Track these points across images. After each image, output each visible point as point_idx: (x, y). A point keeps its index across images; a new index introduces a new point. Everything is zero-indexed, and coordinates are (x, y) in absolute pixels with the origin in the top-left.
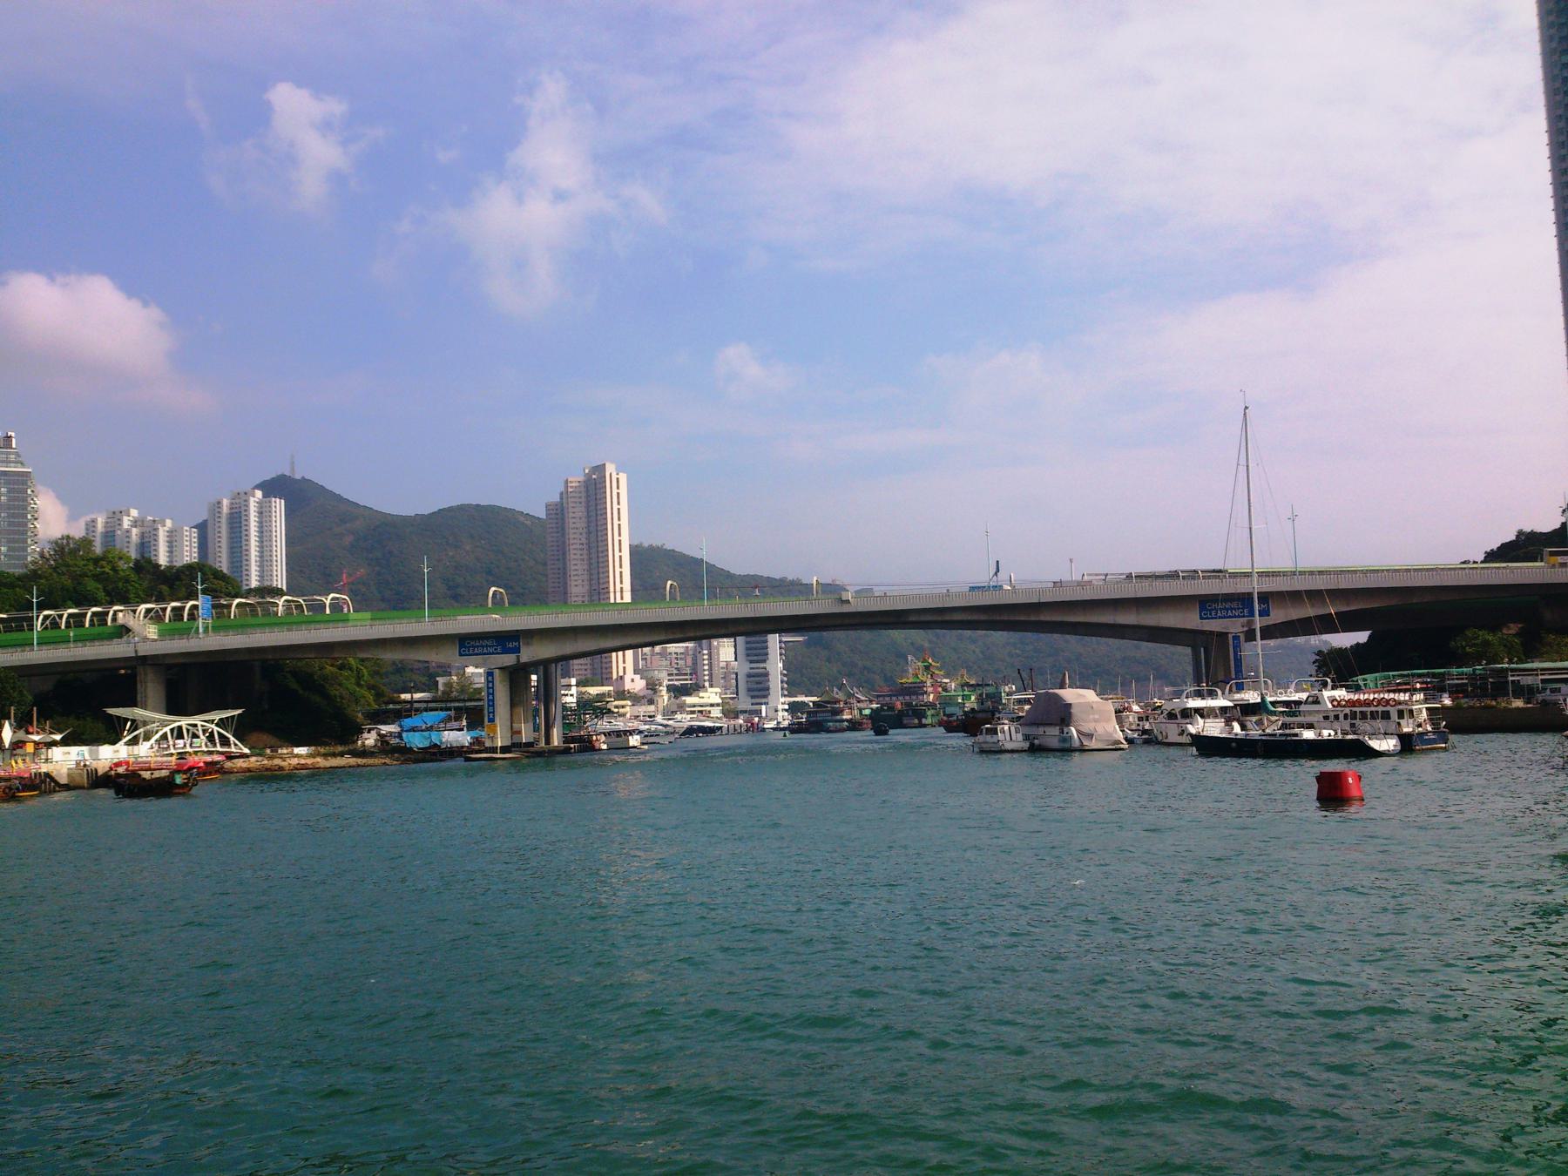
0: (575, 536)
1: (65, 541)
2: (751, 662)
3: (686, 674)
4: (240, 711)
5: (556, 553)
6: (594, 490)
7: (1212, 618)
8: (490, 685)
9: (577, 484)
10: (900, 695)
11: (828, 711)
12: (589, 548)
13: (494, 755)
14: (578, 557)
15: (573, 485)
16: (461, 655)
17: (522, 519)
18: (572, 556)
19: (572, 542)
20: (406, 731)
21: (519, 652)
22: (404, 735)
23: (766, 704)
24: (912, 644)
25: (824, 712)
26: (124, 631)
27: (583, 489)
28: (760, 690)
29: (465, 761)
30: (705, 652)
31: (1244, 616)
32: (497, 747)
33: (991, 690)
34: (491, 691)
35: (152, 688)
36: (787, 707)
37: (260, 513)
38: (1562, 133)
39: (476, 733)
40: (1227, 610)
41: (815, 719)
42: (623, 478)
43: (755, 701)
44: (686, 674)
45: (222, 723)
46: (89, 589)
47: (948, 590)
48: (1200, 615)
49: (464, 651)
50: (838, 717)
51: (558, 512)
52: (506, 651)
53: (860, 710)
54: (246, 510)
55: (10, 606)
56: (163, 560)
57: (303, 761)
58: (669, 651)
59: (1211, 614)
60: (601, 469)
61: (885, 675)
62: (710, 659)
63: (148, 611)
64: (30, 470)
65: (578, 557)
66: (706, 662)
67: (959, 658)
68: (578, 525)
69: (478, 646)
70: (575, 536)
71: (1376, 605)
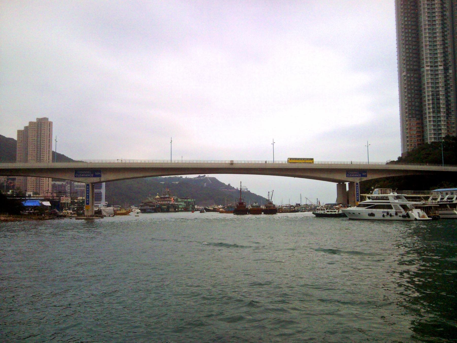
7: (350, 177)
8: (88, 190)
16: (75, 177)
29: (76, 219)
31: (360, 177)
38: (404, 45)
40: (85, 174)
41: (143, 208)
48: (75, 175)
49: (77, 175)
51: (23, 134)
52: (95, 176)
59: (79, 175)
69: (83, 174)
71: (398, 175)
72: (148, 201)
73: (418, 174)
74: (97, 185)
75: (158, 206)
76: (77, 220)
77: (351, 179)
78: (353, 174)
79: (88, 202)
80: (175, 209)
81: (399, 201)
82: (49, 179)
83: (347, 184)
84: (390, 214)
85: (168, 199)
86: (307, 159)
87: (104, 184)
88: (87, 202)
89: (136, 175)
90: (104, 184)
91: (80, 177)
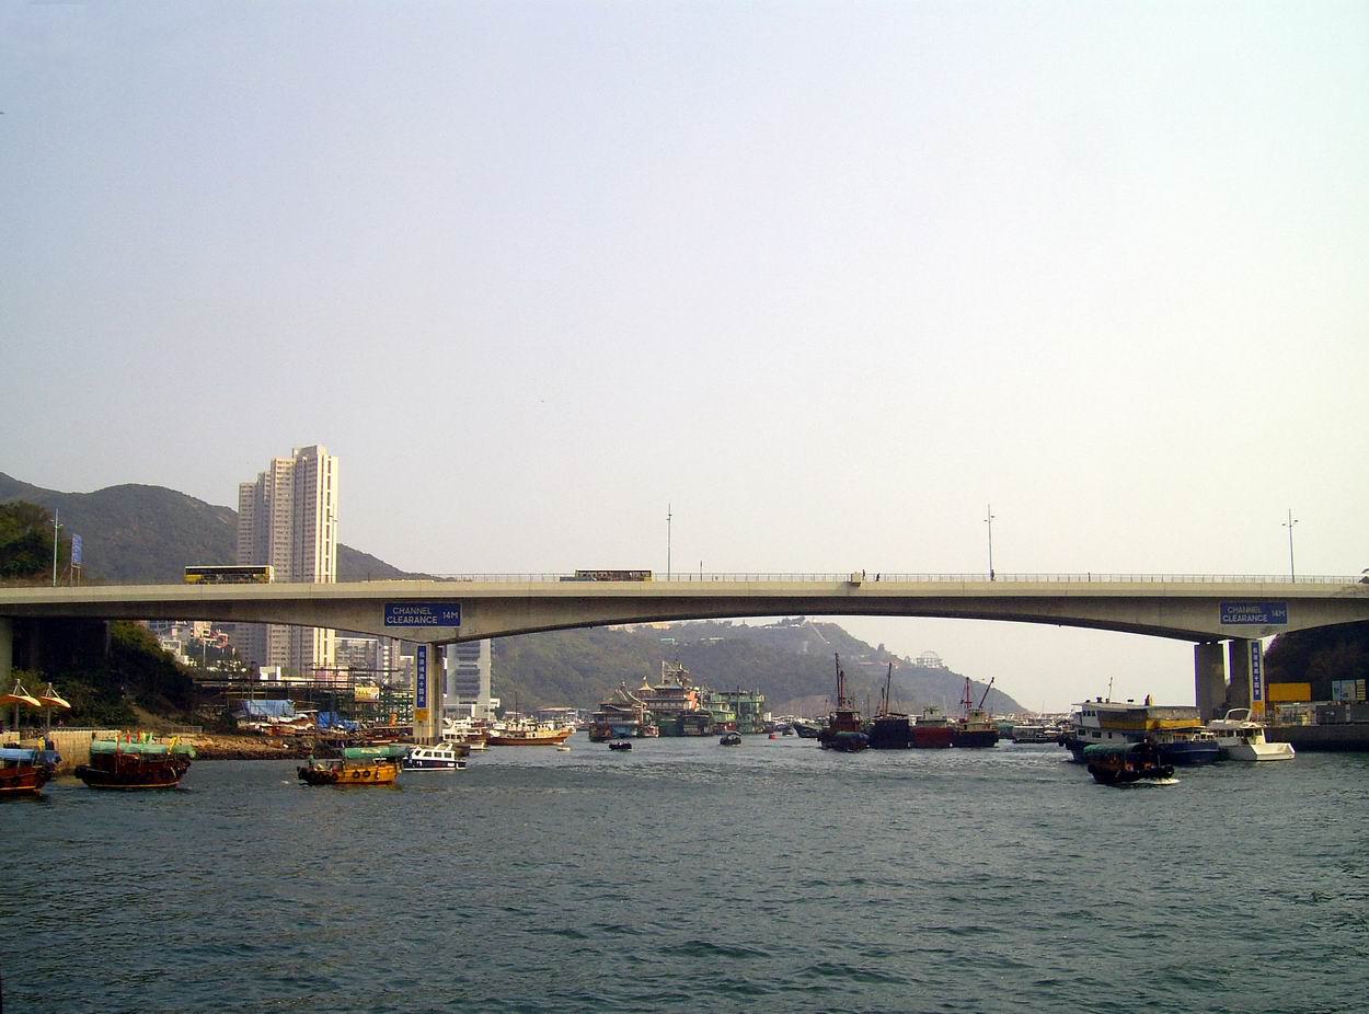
2: (461, 659)
6: (304, 471)
16: (386, 624)
17: (189, 502)
21: (459, 625)
23: (475, 703)
25: (615, 716)
30: (386, 647)
34: (422, 669)
43: (463, 700)
51: (257, 497)
52: (441, 622)
60: (311, 452)
66: (386, 658)
77: (1236, 630)
80: (701, 728)
81: (22, 738)
82: (328, 630)
83: (1226, 644)
84: (193, 754)
85: (676, 697)
91: (401, 625)
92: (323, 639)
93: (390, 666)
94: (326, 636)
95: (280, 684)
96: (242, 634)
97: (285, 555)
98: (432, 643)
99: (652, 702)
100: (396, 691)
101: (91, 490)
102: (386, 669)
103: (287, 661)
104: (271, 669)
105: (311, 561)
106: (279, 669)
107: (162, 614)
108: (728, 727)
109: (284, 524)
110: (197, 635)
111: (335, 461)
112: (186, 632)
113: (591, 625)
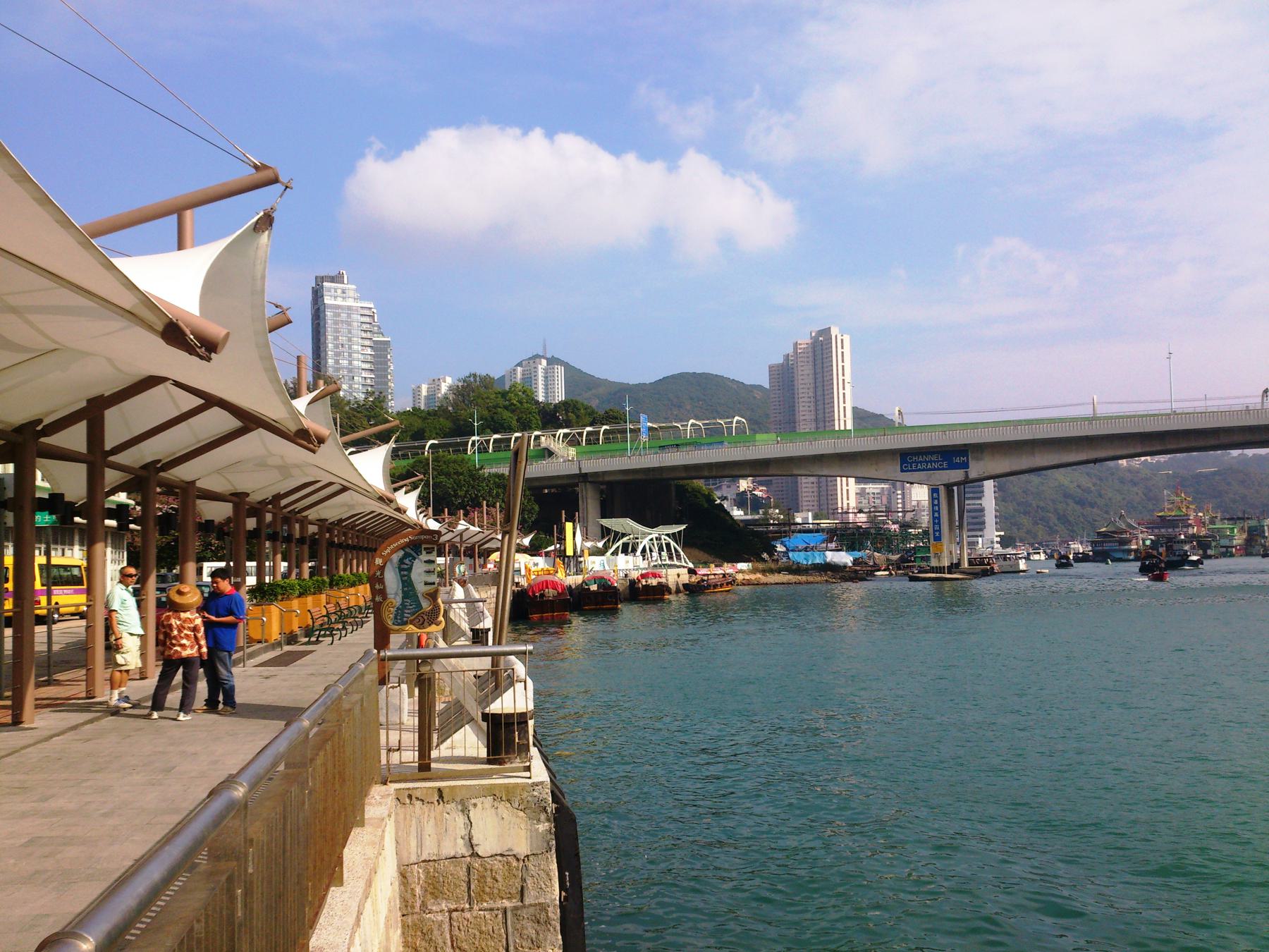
0: (804, 391)
1: (472, 379)
3: (883, 512)
4: (683, 527)
5: (778, 407)
6: (821, 349)
8: (936, 502)
9: (805, 346)
10: (1163, 528)
11: (1116, 541)
12: (816, 401)
13: (943, 575)
14: (806, 408)
15: (802, 346)
16: (902, 471)
18: (801, 409)
19: (800, 396)
20: (792, 551)
22: (791, 554)
23: (981, 536)
24: (1079, 486)
25: (1110, 542)
26: (549, 453)
27: (810, 350)
28: (976, 524)
29: (910, 581)
30: (899, 492)
32: (944, 567)
33: (1253, 523)
35: (590, 503)
36: (998, 539)
37: (546, 378)
39: (858, 554)
40: (927, 462)
41: (1100, 548)
42: (847, 339)
44: (883, 512)
45: (673, 536)
46: (505, 417)
47: (63, 555)
49: (905, 467)
50: (1126, 547)
51: (784, 374)
52: (952, 467)
53: (1144, 541)
54: (535, 376)
55: (437, 434)
56: (541, 398)
57: (747, 577)
58: (867, 491)
60: (826, 332)
61: (1058, 514)
62: (903, 498)
63: (566, 435)
64: (389, 339)
65: (806, 408)
67: (1124, 499)
68: (806, 381)
69: (921, 462)
70: (804, 391)
72: (1114, 529)
73: (630, 477)
74: (971, 485)
75: (1148, 543)
76: (913, 583)
78: (921, 462)
79: (937, 534)
86: (1029, 420)
87: (989, 486)
88: (934, 535)
89: (1025, 462)
90: (989, 486)
92: (845, 488)
93: (903, 507)
94: (847, 485)
95: (811, 526)
96: (778, 487)
97: (809, 407)
98: (944, 485)
99: (1156, 528)
100: (911, 528)
101: (649, 377)
102: (900, 510)
103: (816, 507)
104: (803, 514)
105: (832, 423)
106: (810, 514)
107: (714, 473)
108: (1236, 549)
109: (811, 494)
110: (742, 489)
111: (847, 339)
112: (733, 487)
113: (1095, 461)
